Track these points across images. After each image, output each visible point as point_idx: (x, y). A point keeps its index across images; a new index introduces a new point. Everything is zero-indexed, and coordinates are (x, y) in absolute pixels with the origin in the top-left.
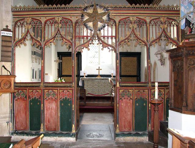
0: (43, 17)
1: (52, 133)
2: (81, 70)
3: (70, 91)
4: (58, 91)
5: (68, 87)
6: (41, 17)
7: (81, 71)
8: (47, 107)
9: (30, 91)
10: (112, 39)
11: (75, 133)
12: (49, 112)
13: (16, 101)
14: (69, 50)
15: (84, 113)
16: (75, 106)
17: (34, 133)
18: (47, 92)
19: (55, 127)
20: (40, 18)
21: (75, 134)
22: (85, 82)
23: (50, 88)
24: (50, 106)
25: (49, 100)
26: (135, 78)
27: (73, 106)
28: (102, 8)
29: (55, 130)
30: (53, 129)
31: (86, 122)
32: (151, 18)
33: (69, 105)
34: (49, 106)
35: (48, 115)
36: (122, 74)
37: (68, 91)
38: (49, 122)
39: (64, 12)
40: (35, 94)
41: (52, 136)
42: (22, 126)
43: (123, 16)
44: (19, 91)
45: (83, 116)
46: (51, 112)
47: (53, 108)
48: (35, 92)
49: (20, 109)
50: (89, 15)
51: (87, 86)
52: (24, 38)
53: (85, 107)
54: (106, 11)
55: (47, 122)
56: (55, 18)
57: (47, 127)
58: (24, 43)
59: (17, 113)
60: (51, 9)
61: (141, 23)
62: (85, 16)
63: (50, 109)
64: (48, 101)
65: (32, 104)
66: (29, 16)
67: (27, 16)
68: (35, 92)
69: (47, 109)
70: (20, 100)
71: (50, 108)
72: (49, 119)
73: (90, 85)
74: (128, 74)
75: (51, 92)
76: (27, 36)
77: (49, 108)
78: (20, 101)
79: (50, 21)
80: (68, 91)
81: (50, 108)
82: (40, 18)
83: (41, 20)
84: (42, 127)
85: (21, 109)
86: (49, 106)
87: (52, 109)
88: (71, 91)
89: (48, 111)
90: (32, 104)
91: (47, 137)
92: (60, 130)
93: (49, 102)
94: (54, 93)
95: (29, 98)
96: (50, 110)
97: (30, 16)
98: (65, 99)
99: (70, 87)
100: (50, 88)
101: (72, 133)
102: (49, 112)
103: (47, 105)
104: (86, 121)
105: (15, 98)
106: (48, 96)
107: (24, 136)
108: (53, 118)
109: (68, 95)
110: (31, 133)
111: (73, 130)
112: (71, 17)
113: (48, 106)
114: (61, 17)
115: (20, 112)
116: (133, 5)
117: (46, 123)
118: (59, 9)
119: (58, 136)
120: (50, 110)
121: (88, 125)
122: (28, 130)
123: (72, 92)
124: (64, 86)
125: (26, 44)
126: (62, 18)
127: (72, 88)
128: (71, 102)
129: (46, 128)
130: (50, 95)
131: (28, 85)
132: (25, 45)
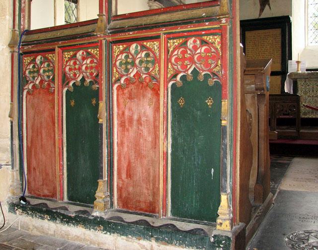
1: (136, 223)
2: (291, 59)
3: (210, 38)
4: (160, 48)
5: (200, 20)
7: (289, 61)
8: (123, 113)
9: (67, 55)
11: (230, 235)
13: (29, 96)
14: (260, 15)
15: (294, 157)
16: (233, 104)
17: (74, 215)
18: (122, 52)
19: (151, 198)
21: (228, 238)
22: (300, 84)
23: (131, 35)
24: (134, 108)
25: (132, 87)
27: (225, 105)
29: (151, 210)
30: (143, 206)
31: (295, 183)
33: (209, 103)
34: (130, 109)
35: (126, 149)
37: (204, 43)
40: (80, 66)
41: (133, 234)
42: (47, 185)
44: (34, 60)
45: (288, 164)
46: (139, 135)
47: (144, 119)
48: (84, 59)
49: (41, 123)
51: (305, 93)
53: (299, 142)
55: (124, 176)
57: (124, 195)
59: (32, 136)
63: (135, 123)
64: (126, 91)
65: (72, 104)
68: (84, 59)
69: (122, 125)
70: (39, 93)
71: (135, 117)
73: (313, 91)
75: (137, 53)
77: (131, 120)
78: (41, 96)
80: (204, 43)
81: (135, 117)
84: (101, 193)
85: (44, 124)
87: (141, 124)
88: (218, 39)
89: (128, 130)
91: (116, 235)
92: (169, 214)
93: (130, 94)
94: (147, 55)
95: (63, 81)
96: (135, 127)
98: (190, 78)
99: (209, 19)
100: (131, 35)
101: (215, 233)
102: (132, 133)
103: (122, 106)
104: (297, 179)
105: (26, 87)
106: (127, 70)
107: (43, 218)
108: (145, 162)
109: (204, 59)
110: (62, 212)
111: (219, 221)
113: (127, 113)
115: (41, 133)
117: (119, 177)
119: (157, 240)
120: (135, 127)
121: (301, 193)
122: (62, 199)
123: (222, 43)
124: (186, 17)
127: (219, 20)
128: (217, 91)
129: (120, 197)
130: (133, 64)
131: (58, 34)
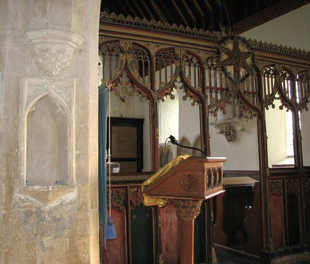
0: (153, 44)
6: (150, 43)
10: (217, 92)
12: (167, 229)
20: (149, 45)
26: (291, 152)
28: (246, 46)
32: (298, 69)
36: (113, 157)
38: (167, 250)
39: (190, 40)
43: (165, 44)
50: (228, 52)
52: (172, 86)
54: (250, 51)
56: (118, 41)
58: (187, 95)
60: (123, 22)
61: (140, 54)
62: (223, 53)
63: (169, 224)
66: (127, 37)
67: (122, 36)
71: (169, 221)
72: (167, 244)
74: (122, 157)
76: (121, 76)
77: (167, 223)
79: (106, 46)
81: (169, 221)
82: (149, 45)
83: (149, 48)
86: (166, 218)
90: (134, 217)
97: (129, 37)
112: (199, 52)
113: (165, 220)
114: (185, 49)
116: (121, 15)
118: (174, 32)
125: (173, 95)
126: (133, 43)
132: (173, 97)
